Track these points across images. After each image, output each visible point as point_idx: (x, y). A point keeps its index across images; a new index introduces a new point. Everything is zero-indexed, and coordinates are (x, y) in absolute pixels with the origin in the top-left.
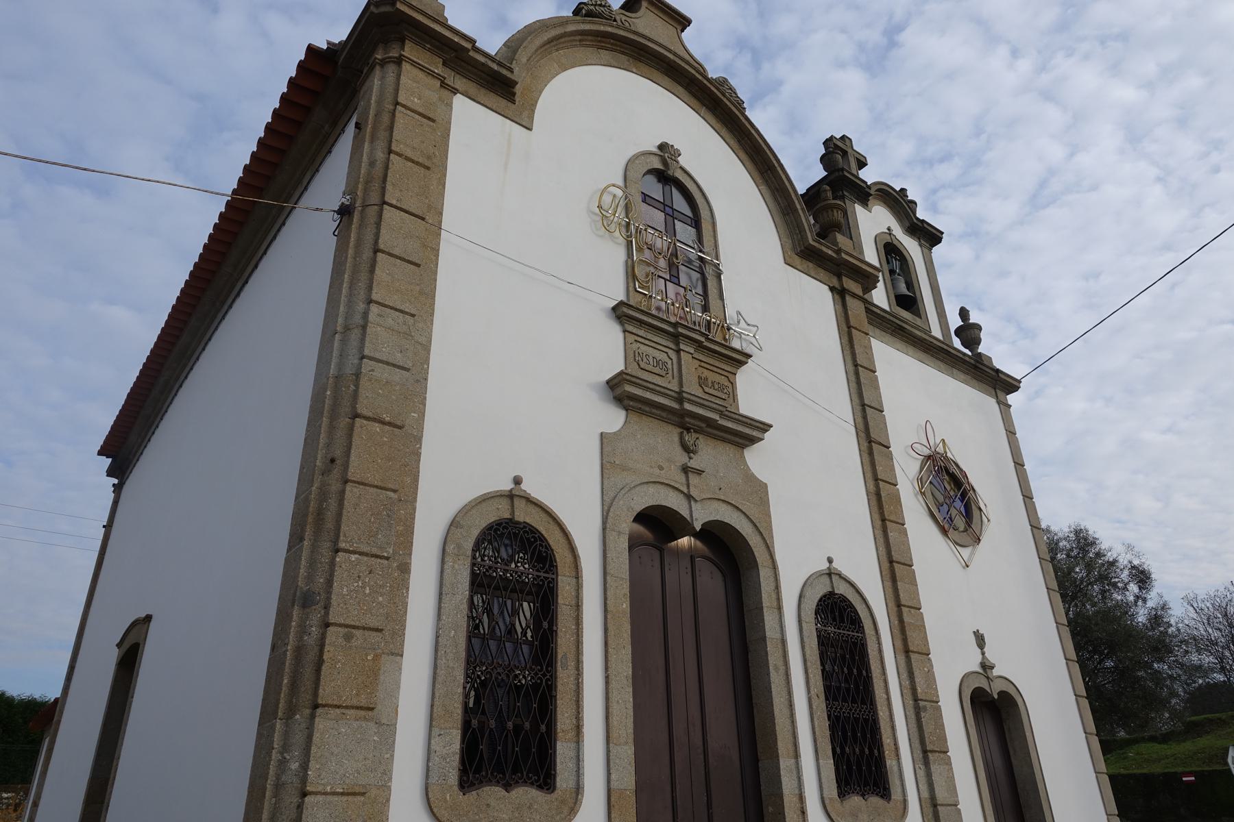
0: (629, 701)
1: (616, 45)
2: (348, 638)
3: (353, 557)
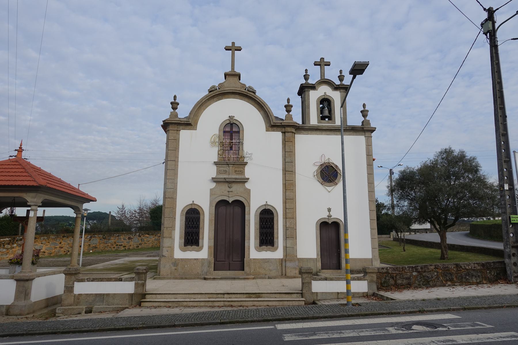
2: (167, 229)
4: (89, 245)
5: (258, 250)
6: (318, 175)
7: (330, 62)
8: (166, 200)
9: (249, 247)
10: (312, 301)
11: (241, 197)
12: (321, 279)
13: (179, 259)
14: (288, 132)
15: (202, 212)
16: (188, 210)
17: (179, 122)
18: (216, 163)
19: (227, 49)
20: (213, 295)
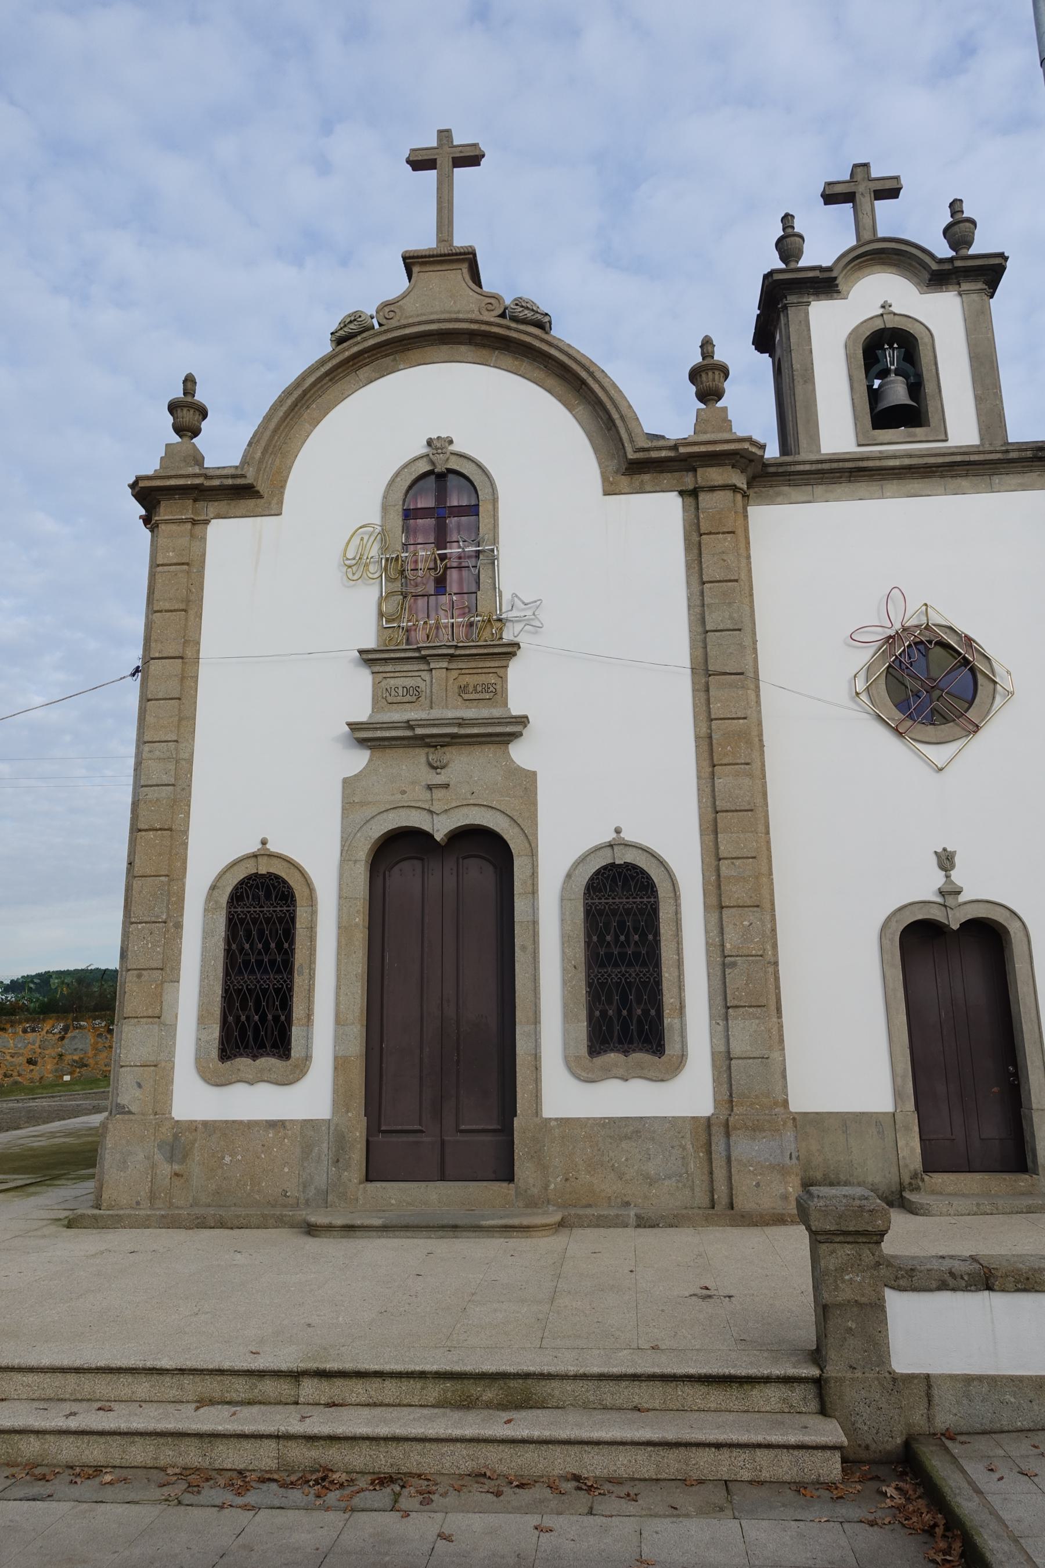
0: (357, 993)
1: (373, 355)
2: (139, 976)
3: (140, 926)
4: (61, 1055)
5: (584, 1074)
6: (873, 691)
7: (897, 178)
8: (138, 841)
9: (537, 1057)
10: (899, 1441)
11: (491, 812)
12: (947, 1277)
13: (193, 1126)
14: (712, 489)
15: (307, 891)
16: (242, 882)
17: (197, 481)
18: (368, 658)
19: (420, 163)
20: (227, 1380)
